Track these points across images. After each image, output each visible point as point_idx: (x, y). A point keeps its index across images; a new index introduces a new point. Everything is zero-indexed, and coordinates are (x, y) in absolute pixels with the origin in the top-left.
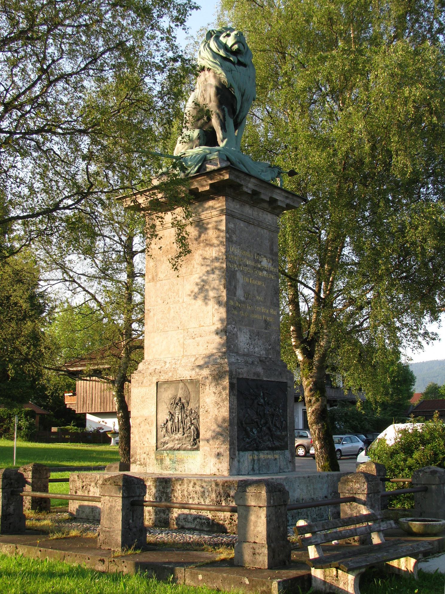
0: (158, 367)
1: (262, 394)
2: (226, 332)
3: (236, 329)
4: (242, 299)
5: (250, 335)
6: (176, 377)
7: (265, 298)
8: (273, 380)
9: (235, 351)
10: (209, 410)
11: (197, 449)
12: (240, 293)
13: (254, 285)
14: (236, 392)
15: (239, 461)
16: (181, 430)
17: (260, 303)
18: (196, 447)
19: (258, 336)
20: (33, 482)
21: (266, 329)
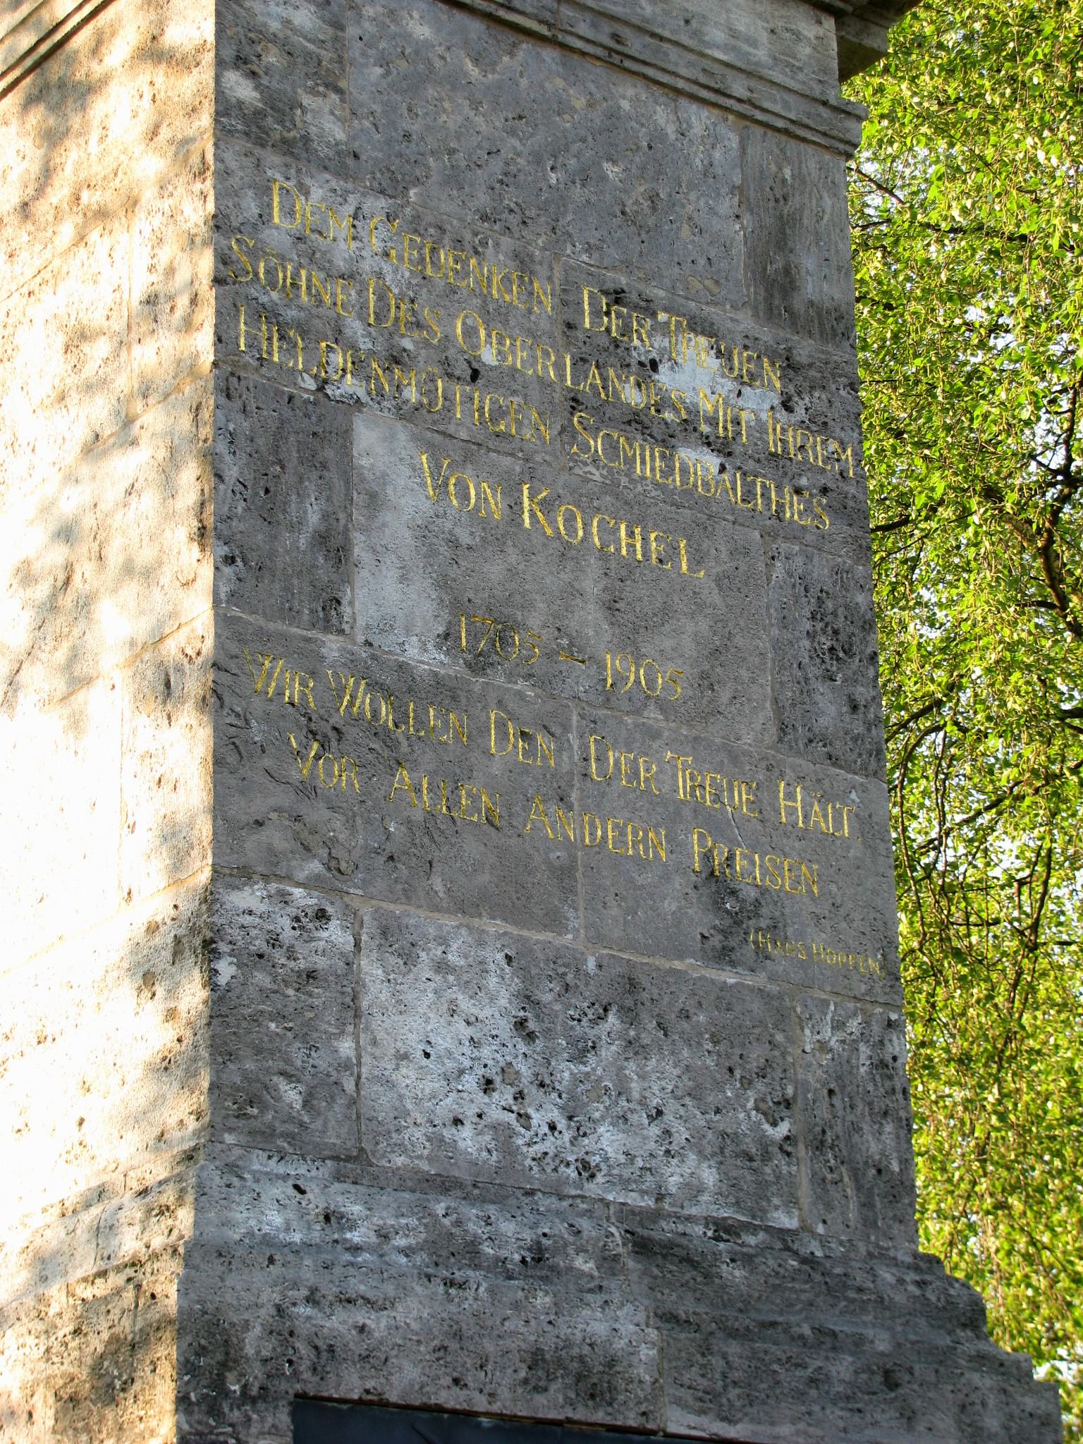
2: (209, 950)
3: (336, 934)
5: (527, 999)
7: (706, 682)
9: (336, 1136)
13: (566, 553)
17: (652, 715)
19: (630, 1015)
21: (724, 956)
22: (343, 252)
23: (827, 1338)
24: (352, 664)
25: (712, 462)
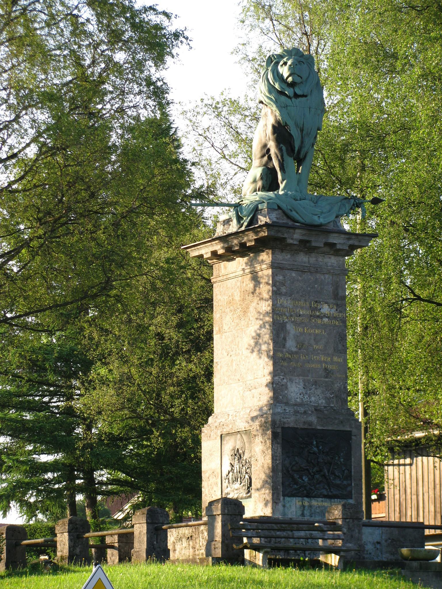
0: (223, 420)
1: (315, 443)
3: (285, 380)
4: (294, 349)
5: (305, 385)
6: (235, 430)
7: (325, 346)
8: (330, 428)
9: (285, 401)
10: (258, 459)
11: (250, 497)
12: (291, 344)
13: (310, 334)
14: (280, 440)
15: (284, 506)
16: (239, 479)
17: (319, 351)
18: (249, 495)
19: (316, 385)
20: (119, 546)
21: (326, 377)
23: (336, 418)
24: (287, 352)
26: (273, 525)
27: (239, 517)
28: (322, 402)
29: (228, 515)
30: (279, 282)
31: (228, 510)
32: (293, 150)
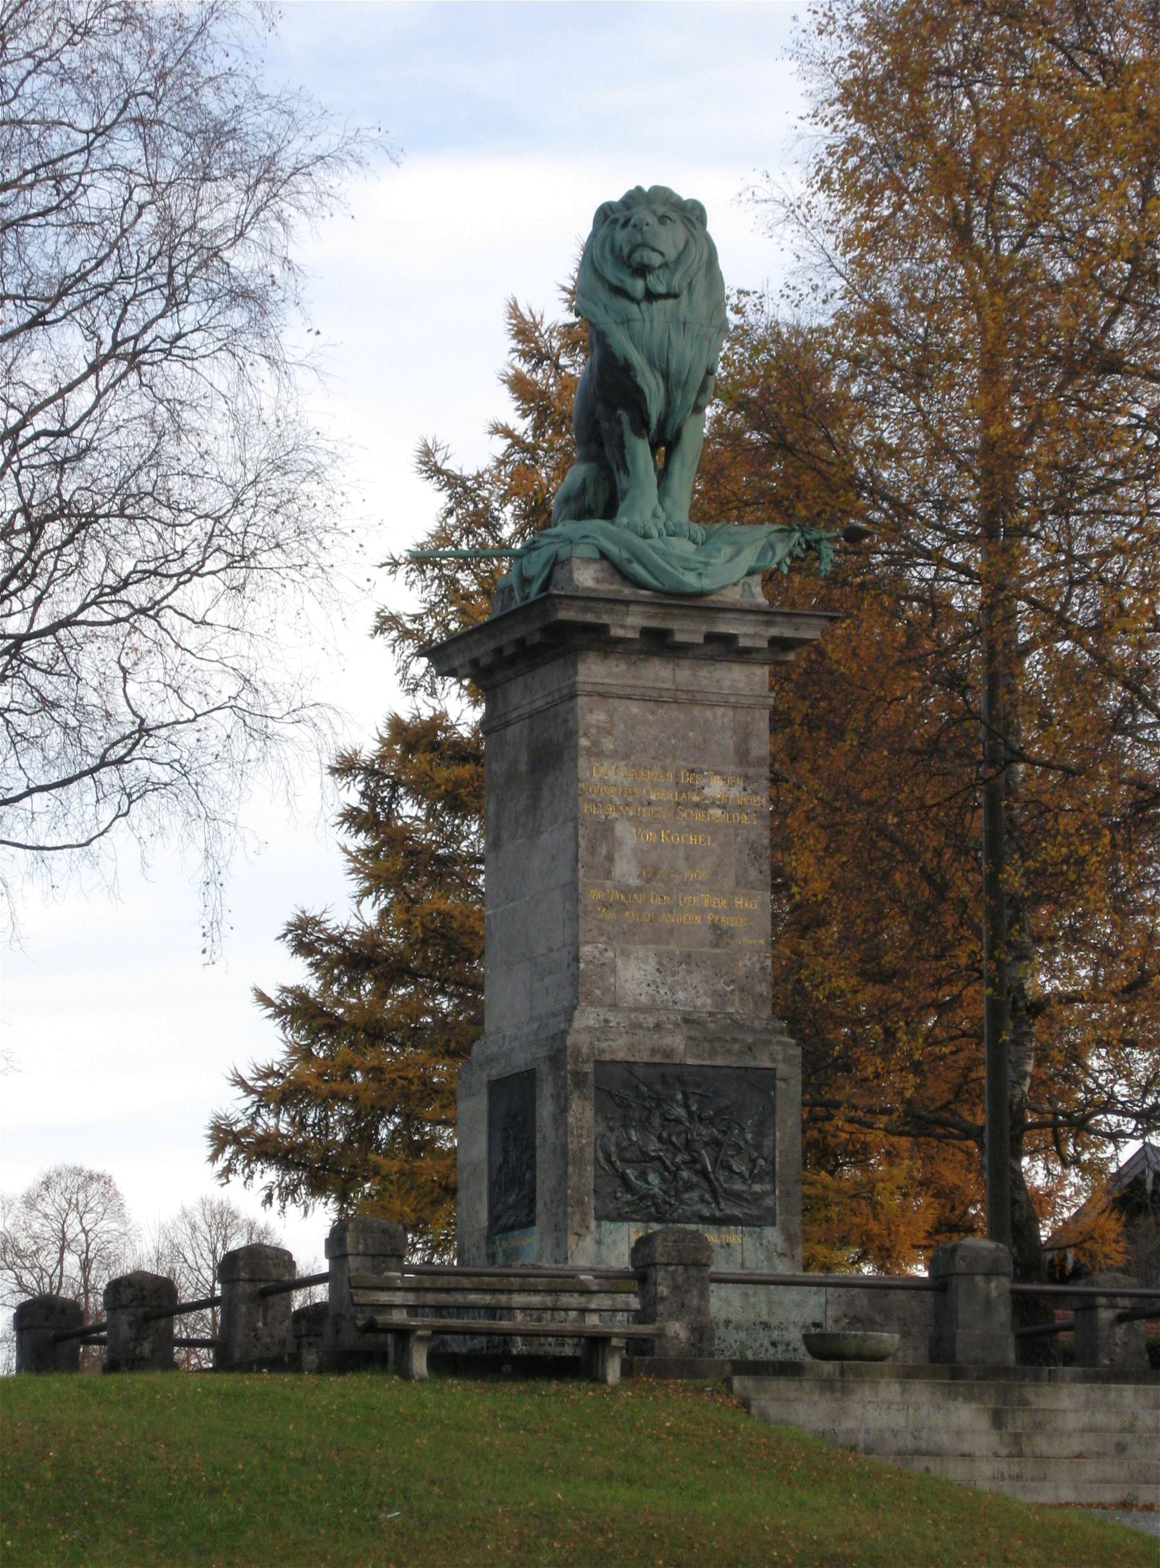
1: (680, 1096)
3: (610, 954)
4: (634, 881)
5: (660, 963)
7: (715, 873)
9: (609, 999)
15: (599, 1242)
17: (698, 885)
19: (688, 964)
21: (716, 945)
22: (613, 779)
23: (735, 1040)
24: (615, 887)
25: (719, 812)
26: (461, 1279)
27: (394, 1261)
28: (705, 1003)
29: (365, 1255)
30: (598, 727)
31: (366, 1245)
32: (646, 423)
